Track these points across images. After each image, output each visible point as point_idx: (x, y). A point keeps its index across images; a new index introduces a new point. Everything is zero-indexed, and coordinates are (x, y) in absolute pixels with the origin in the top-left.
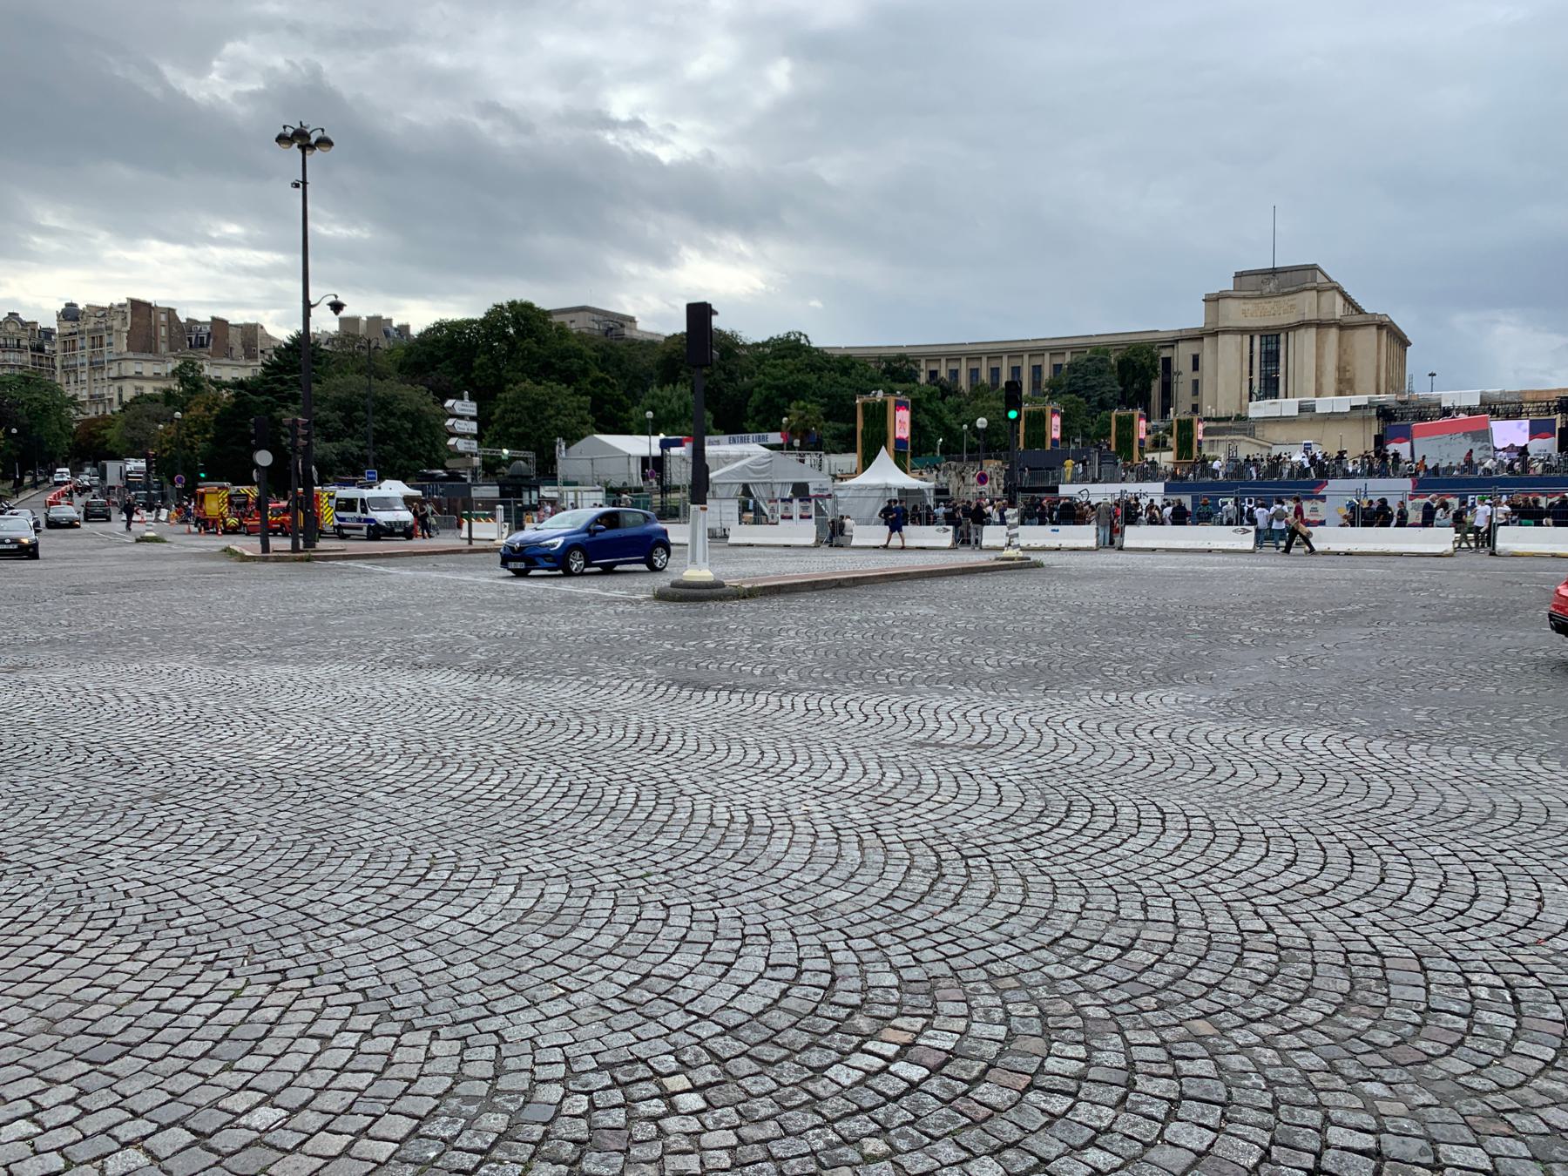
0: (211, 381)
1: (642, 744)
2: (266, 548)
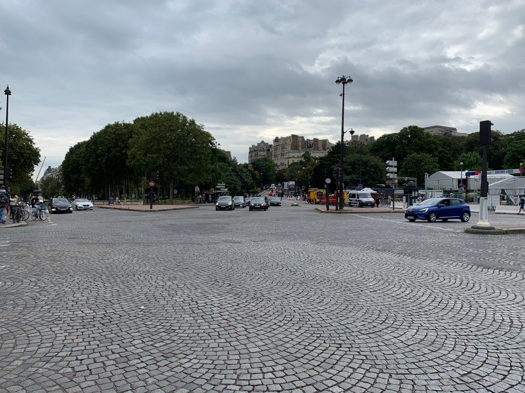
0: (314, 158)
1: (462, 286)
2: (328, 209)
